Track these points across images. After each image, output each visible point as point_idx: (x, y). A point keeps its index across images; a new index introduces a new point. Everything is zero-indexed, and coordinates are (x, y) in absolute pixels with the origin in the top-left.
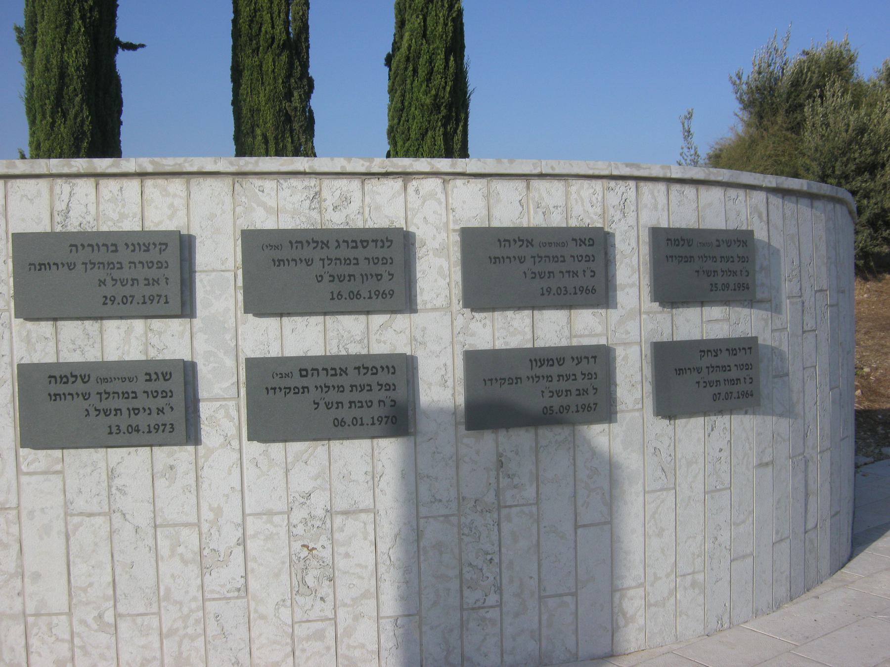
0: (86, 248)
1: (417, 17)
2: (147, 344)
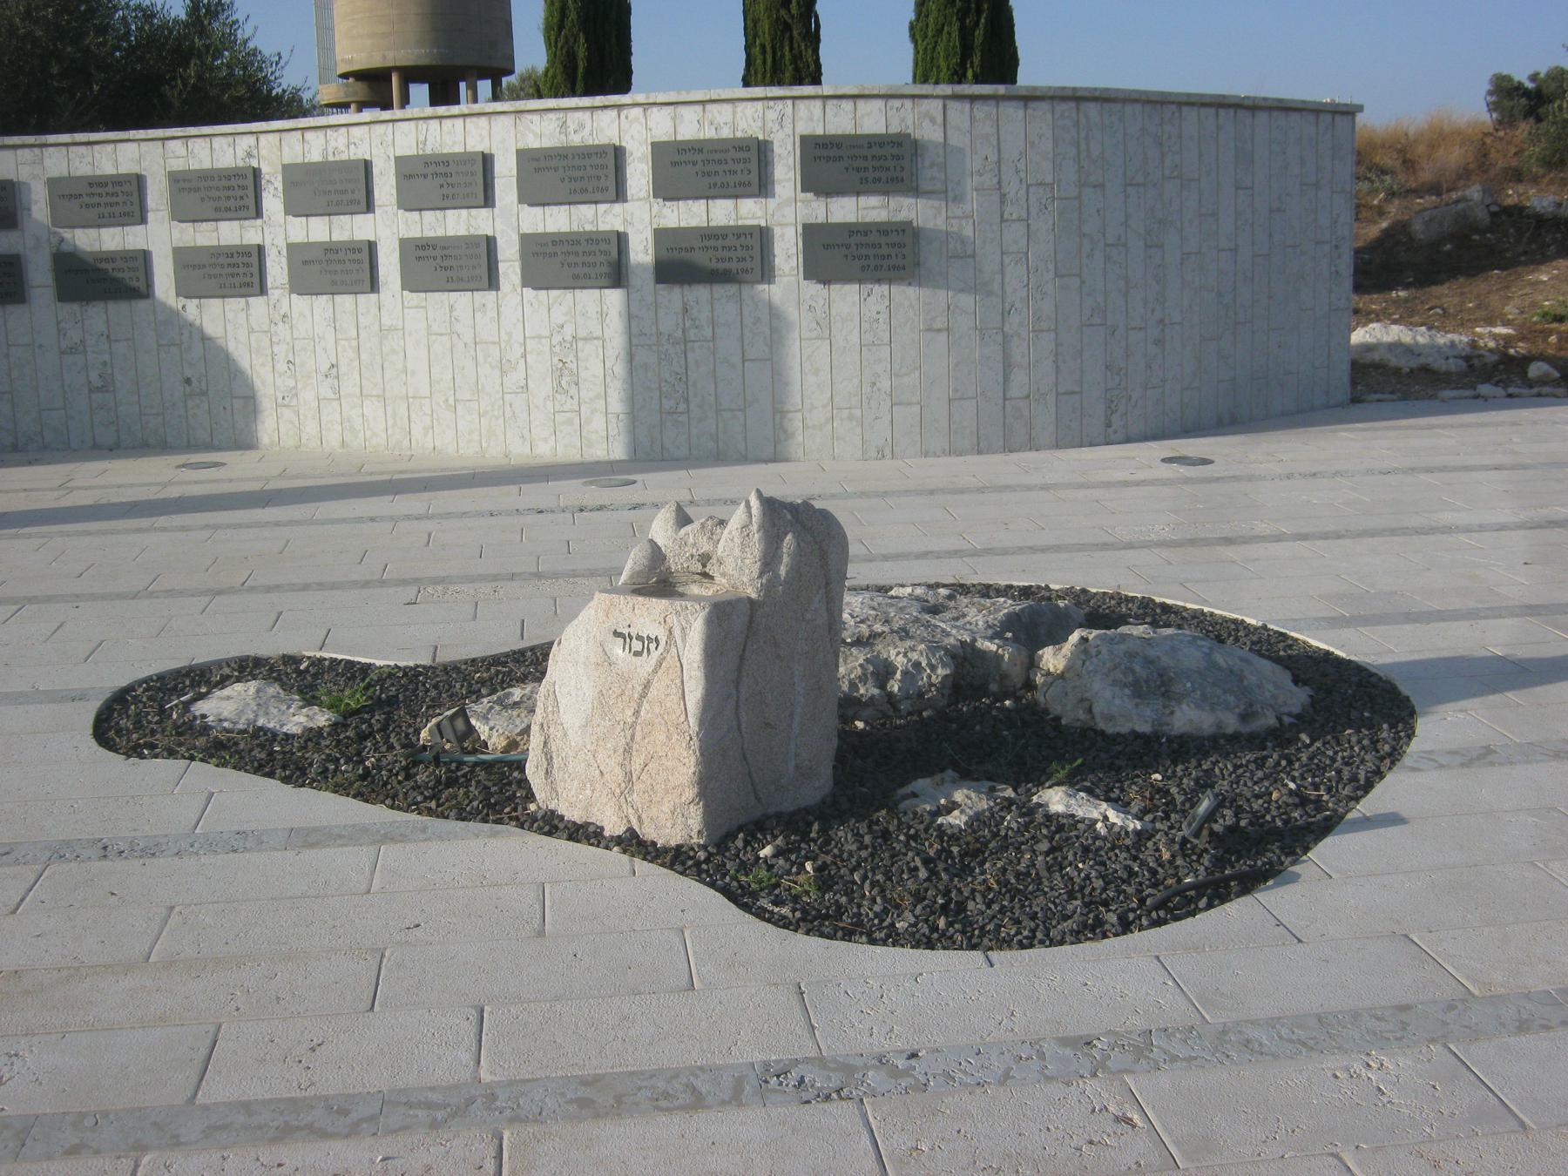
2: (469, 225)
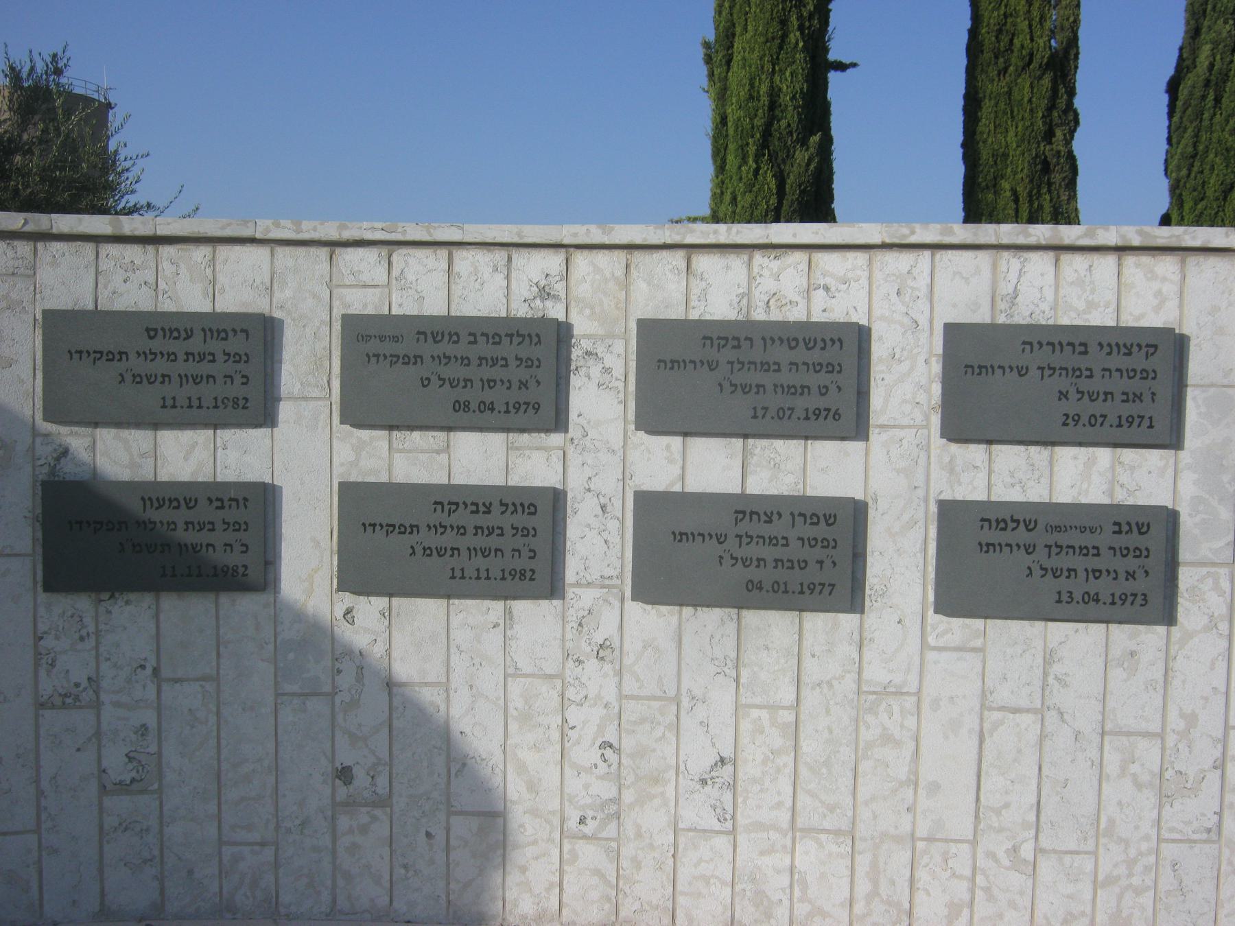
0: (1045, 347)
1: (1226, 22)
2: (1113, 482)
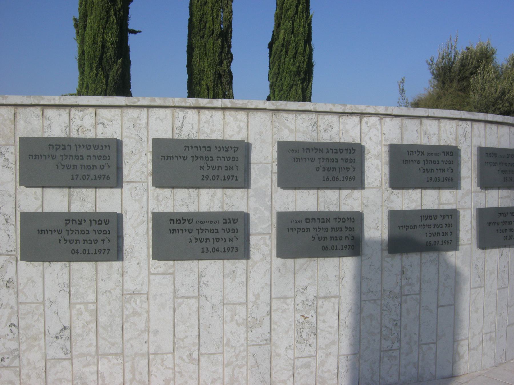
1: (289, 22)
2: (223, 202)
